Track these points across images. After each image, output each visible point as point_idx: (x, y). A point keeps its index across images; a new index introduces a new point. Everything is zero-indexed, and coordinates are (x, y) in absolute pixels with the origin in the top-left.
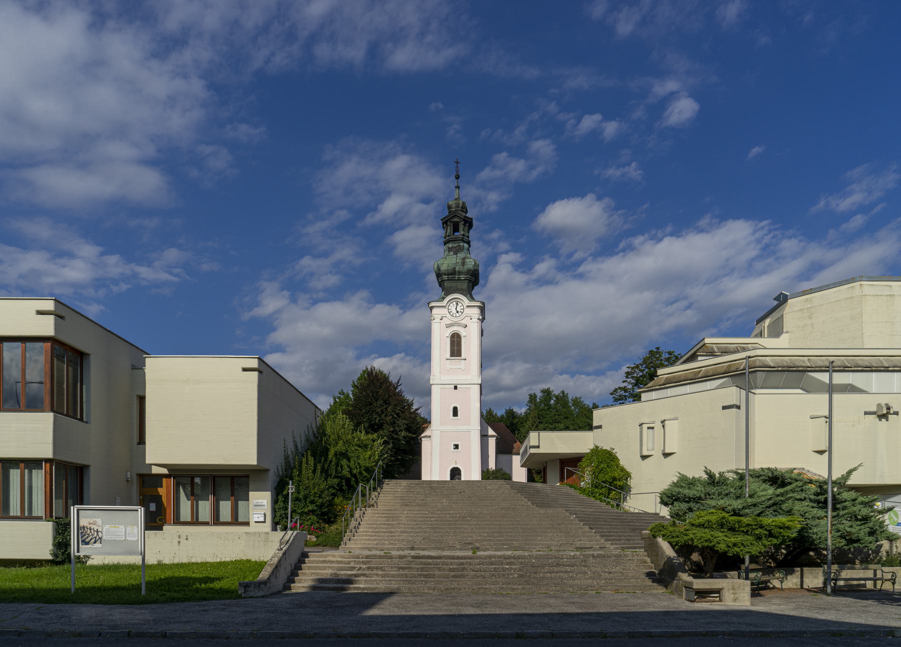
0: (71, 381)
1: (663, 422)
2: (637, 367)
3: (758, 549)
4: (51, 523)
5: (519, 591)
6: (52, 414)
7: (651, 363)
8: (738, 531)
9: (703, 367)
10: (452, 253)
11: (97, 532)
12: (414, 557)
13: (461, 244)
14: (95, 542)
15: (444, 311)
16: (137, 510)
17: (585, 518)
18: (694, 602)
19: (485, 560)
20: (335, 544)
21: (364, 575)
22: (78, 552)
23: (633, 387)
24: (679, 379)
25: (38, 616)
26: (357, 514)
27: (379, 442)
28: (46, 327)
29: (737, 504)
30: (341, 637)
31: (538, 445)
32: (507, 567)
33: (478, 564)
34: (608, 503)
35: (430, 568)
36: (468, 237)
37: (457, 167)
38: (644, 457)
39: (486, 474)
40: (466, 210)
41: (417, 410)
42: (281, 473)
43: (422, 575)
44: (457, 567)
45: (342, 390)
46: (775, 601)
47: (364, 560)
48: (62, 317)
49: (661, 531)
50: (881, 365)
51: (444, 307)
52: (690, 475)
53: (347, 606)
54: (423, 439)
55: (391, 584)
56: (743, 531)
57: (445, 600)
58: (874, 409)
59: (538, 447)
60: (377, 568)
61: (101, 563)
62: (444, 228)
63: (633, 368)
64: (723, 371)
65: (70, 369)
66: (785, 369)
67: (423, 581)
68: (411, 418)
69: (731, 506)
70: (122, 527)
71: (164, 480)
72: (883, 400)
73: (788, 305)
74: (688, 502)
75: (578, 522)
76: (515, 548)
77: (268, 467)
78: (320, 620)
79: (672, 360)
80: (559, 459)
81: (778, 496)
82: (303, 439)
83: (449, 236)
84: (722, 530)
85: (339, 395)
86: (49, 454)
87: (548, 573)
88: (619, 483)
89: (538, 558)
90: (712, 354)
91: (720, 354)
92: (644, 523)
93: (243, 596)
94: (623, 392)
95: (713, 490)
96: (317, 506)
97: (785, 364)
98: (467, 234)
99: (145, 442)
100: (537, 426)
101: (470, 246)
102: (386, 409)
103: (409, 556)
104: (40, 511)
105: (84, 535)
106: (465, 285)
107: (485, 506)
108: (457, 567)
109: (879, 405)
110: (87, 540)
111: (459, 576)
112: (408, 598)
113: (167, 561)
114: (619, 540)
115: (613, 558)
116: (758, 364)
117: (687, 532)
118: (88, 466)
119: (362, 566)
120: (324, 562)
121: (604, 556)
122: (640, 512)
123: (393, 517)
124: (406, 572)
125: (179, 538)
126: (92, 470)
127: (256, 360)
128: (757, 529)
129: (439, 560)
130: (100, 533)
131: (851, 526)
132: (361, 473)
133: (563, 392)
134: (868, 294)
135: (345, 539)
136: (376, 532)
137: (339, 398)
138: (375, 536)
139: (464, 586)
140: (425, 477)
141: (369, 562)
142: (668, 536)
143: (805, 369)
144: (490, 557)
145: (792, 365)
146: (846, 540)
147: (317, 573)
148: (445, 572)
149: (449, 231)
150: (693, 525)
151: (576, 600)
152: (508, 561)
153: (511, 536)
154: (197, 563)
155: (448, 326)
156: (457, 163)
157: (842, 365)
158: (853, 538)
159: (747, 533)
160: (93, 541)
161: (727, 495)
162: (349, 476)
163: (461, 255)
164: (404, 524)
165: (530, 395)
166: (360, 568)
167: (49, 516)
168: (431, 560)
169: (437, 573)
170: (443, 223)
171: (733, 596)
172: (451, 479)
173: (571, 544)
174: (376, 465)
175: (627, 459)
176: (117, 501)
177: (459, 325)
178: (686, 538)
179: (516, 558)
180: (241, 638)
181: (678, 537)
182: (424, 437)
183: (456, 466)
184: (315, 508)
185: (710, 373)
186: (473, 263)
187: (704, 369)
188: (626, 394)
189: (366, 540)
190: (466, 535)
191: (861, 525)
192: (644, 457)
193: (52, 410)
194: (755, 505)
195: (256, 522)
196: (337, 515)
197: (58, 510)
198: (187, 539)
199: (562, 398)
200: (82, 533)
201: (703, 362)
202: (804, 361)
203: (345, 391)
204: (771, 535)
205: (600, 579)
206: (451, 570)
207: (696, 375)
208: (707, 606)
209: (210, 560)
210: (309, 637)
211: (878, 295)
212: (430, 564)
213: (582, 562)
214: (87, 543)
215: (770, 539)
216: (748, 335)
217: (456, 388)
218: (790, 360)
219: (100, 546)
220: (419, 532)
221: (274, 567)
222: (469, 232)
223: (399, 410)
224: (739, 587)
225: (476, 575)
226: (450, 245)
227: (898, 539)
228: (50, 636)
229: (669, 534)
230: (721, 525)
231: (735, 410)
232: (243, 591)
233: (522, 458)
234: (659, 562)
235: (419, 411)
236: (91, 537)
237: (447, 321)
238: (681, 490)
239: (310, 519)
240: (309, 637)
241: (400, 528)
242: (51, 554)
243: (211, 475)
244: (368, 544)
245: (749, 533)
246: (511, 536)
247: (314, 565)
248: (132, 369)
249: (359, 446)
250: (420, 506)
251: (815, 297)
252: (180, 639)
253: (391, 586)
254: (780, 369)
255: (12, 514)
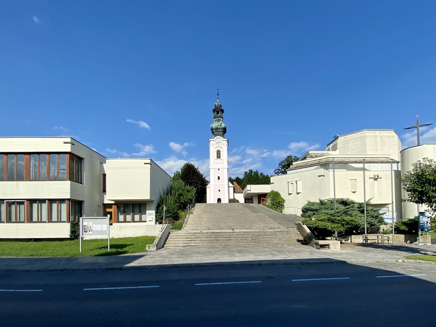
0: (77, 169)
1: (296, 181)
2: (283, 162)
3: (343, 229)
4: (69, 224)
5: (252, 246)
6: (70, 182)
7: (288, 160)
8: (335, 222)
9: (310, 162)
10: (216, 122)
11: (90, 227)
12: (211, 233)
13: (220, 119)
14: (89, 231)
15: (214, 142)
16: (107, 218)
17: (271, 217)
18: (319, 249)
19: (238, 234)
20: (180, 228)
21: (193, 240)
22: (83, 235)
23: (282, 169)
24: (301, 166)
25: (68, 263)
26: (187, 216)
27: (194, 190)
28: (68, 148)
29: (332, 212)
30: (191, 267)
31: (250, 190)
32: (247, 236)
33: (236, 235)
34: (277, 211)
35: (218, 237)
36: (222, 116)
37: (218, 91)
38: (290, 194)
39: (230, 201)
40: (221, 106)
41: (205, 177)
42: (158, 202)
43: (215, 240)
44: (228, 236)
45: (177, 171)
46: (348, 248)
47: (193, 234)
48: (73, 144)
49: (306, 222)
50: (374, 161)
51: (214, 141)
52: (312, 201)
53: (189, 253)
54: (207, 188)
55: (204, 244)
56: (337, 222)
57: (226, 250)
58: (373, 177)
59: (250, 190)
60: (198, 238)
61: (90, 239)
62: (213, 113)
63: (281, 162)
64: (317, 163)
65: (77, 166)
66: (340, 162)
67: (216, 242)
68: (203, 180)
69: (330, 213)
70: (100, 225)
71: (113, 206)
72: (376, 173)
73: (339, 140)
74: (313, 211)
75: (269, 218)
76: (247, 228)
77: (154, 200)
78: (181, 260)
79: (297, 159)
80: (258, 195)
81: (347, 209)
82: (166, 189)
83: (215, 116)
84: (329, 222)
85: (176, 173)
86: (69, 197)
87: (262, 238)
88: (281, 204)
89: (258, 232)
90: (312, 157)
91: (315, 157)
92: (292, 218)
93: (148, 251)
94: (278, 170)
95: (322, 207)
96: (172, 214)
97: (340, 160)
98: (222, 115)
99: (106, 192)
100: (247, 183)
101: (223, 119)
102: (194, 177)
103: (210, 233)
104: (65, 219)
105: (85, 229)
106: (221, 133)
107: (234, 212)
108: (228, 236)
109: (374, 175)
110: (86, 231)
111: (229, 240)
112: (211, 249)
113: (115, 237)
114: (284, 225)
115: (286, 232)
116: (330, 160)
117: (316, 223)
118: (83, 201)
119: (192, 237)
120: (178, 236)
121: (282, 231)
122: (290, 214)
123: (201, 217)
124: (209, 239)
125: (120, 228)
126: (85, 202)
127: (150, 160)
128: (342, 221)
129: (221, 234)
130: (91, 228)
131: (372, 220)
132: (188, 201)
133: (257, 171)
134: (368, 135)
135: (183, 226)
136: (195, 223)
137: (176, 174)
138: (195, 225)
139: (232, 244)
140: (208, 201)
141: (195, 235)
142: (309, 224)
143: (347, 162)
144: (240, 232)
145: (342, 161)
146: (370, 225)
147: (175, 240)
148: (224, 239)
149: (215, 114)
150: (318, 220)
151: (275, 249)
152: (247, 233)
153: (245, 224)
154: (127, 238)
155: (215, 148)
156: (218, 89)
157: (360, 161)
158: (373, 224)
159: (338, 223)
160: (89, 231)
161: (327, 208)
162: (184, 202)
163: (220, 122)
164: (205, 220)
165: (245, 172)
166: (192, 237)
167: (68, 221)
168: (218, 234)
169: (221, 239)
170: (213, 111)
171: (334, 247)
172: (218, 203)
173: (267, 227)
174: (193, 198)
175: (284, 195)
176: (95, 214)
177: (220, 147)
178: (316, 225)
179: (250, 233)
180: (152, 269)
181: (313, 224)
182: (207, 187)
183: (219, 198)
184: (172, 215)
185: (312, 164)
186: (224, 125)
187: (310, 162)
188: (279, 171)
189: (191, 226)
190: (228, 223)
191: (375, 219)
192: (290, 194)
193: (70, 180)
194: (338, 212)
195: (149, 221)
196: (179, 217)
197: (72, 218)
198: (123, 228)
199: (256, 173)
200: (84, 228)
201: (308, 160)
202: (346, 159)
203: (178, 171)
204: (348, 224)
205: (282, 240)
206: (226, 238)
207: (307, 164)
208: (325, 251)
209: (132, 236)
210: (179, 268)
211: (371, 136)
212: (218, 235)
213: (274, 234)
214: (86, 232)
215: (348, 225)
216: (324, 150)
217: (219, 169)
218: (341, 159)
219: (92, 233)
220: (211, 223)
221: (159, 238)
222: (222, 114)
223: (198, 178)
224: (336, 243)
225: (235, 239)
226: (216, 119)
227: (388, 224)
228: (74, 271)
229: (309, 224)
230: (329, 220)
231: (323, 177)
232: (148, 249)
233: (244, 195)
234: (303, 234)
235: (205, 178)
236: (88, 230)
237: (215, 146)
238: (310, 207)
239: (170, 219)
240: (179, 268)
241: (204, 221)
242: (69, 236)
243: (131, 203)
244: (192, 228)
245: (339, 223)
246: (245, 224)
247: (174, 237)
248: (101, 164)
249: (187, 191)
250: (210, 213)
251: (348, 137)
252: (127, 270)
253: (204, 244)
254: (338, 162)
255: (53, 220)
